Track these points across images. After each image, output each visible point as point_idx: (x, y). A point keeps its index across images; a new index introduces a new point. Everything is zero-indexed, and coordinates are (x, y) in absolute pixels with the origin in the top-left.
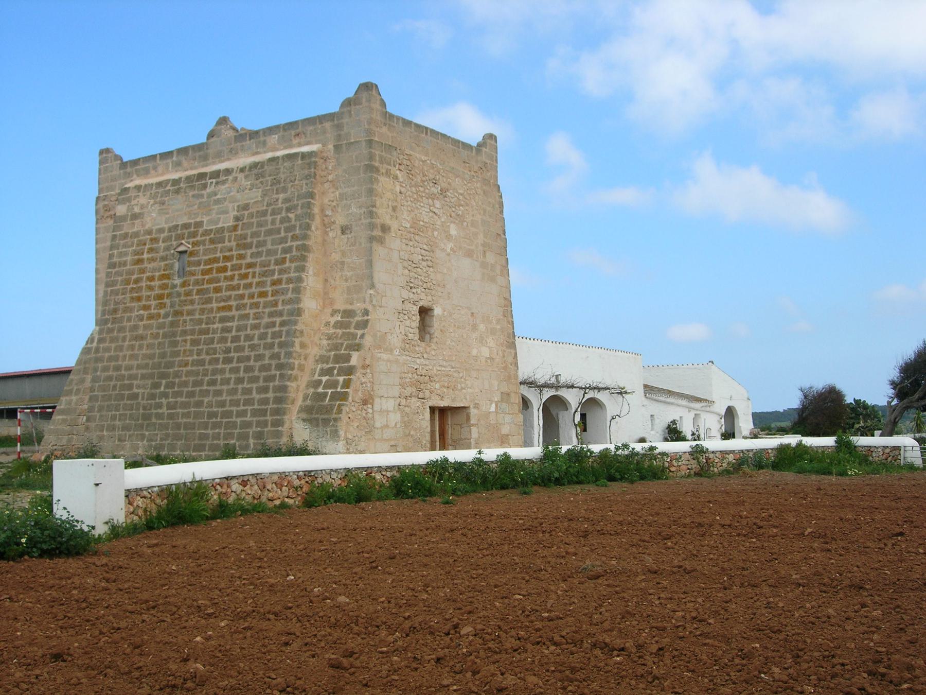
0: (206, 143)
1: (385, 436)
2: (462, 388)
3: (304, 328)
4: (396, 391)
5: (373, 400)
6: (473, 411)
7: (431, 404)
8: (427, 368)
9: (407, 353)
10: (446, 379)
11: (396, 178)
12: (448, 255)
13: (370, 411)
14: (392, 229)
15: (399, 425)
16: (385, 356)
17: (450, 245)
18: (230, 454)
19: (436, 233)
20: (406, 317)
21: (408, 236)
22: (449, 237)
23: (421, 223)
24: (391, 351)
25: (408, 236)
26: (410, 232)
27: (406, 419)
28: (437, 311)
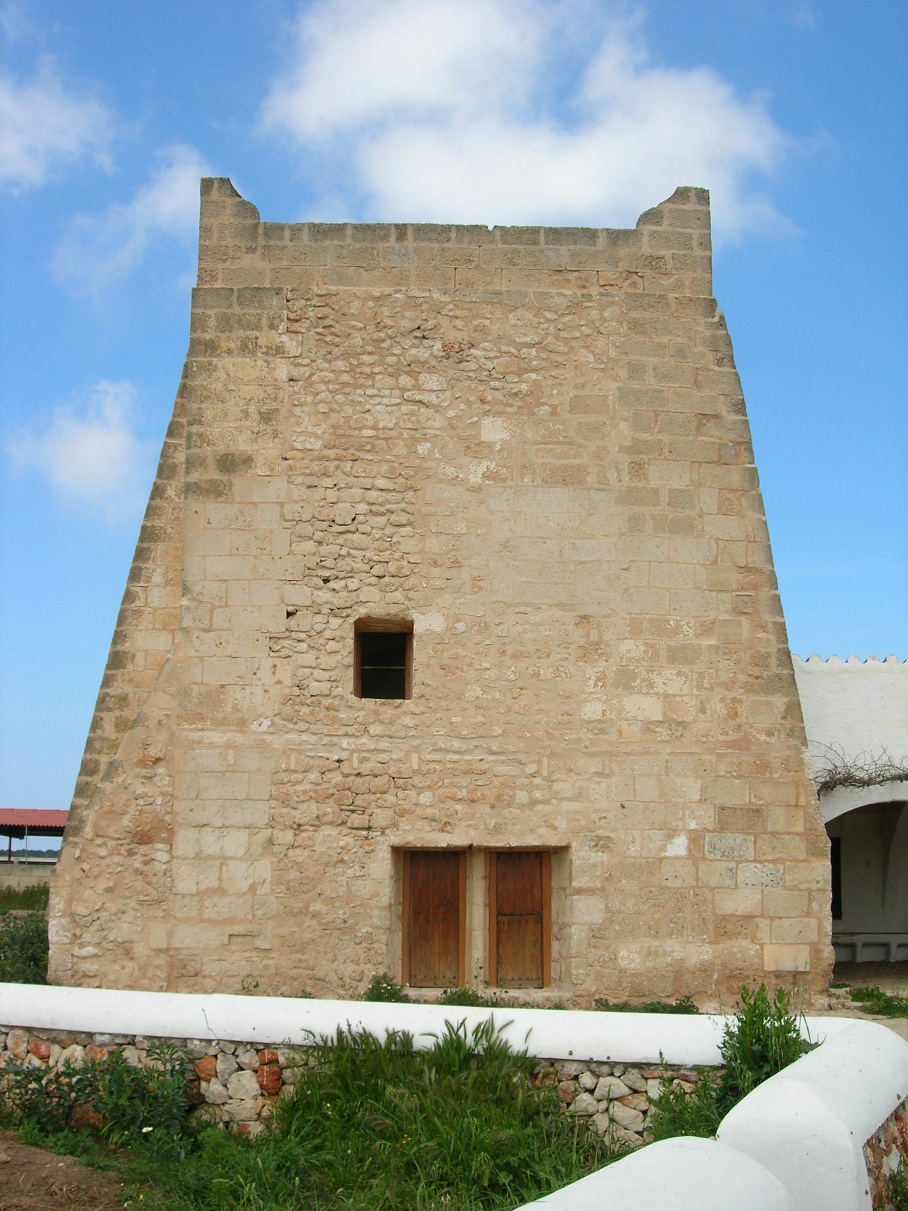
0: (635, 231)
1: (209, 913)
2: (534, 802)
3: (128, 689)
4: (259, 813)
5: (171, 832)
6: (582, 856)
7: (396, 839)
8: (383, 757)
9: (302, 726)
10: (464, 781)
11: (279, 350)
12: (477, 489)
13: (163, 856)
14: (260, 460)
15: (263, 890)
16: (216, 737)
17: (476, 473)
18: (181, 975)
19: (423, 448)
20: (303, 646)
21: (316, 467)
22: (476, 448)
23: (367, 433)
24: (242, 724)
25: (316, 467)
26: (320, 458)
27: (293, 875)
28: (425, 624)
